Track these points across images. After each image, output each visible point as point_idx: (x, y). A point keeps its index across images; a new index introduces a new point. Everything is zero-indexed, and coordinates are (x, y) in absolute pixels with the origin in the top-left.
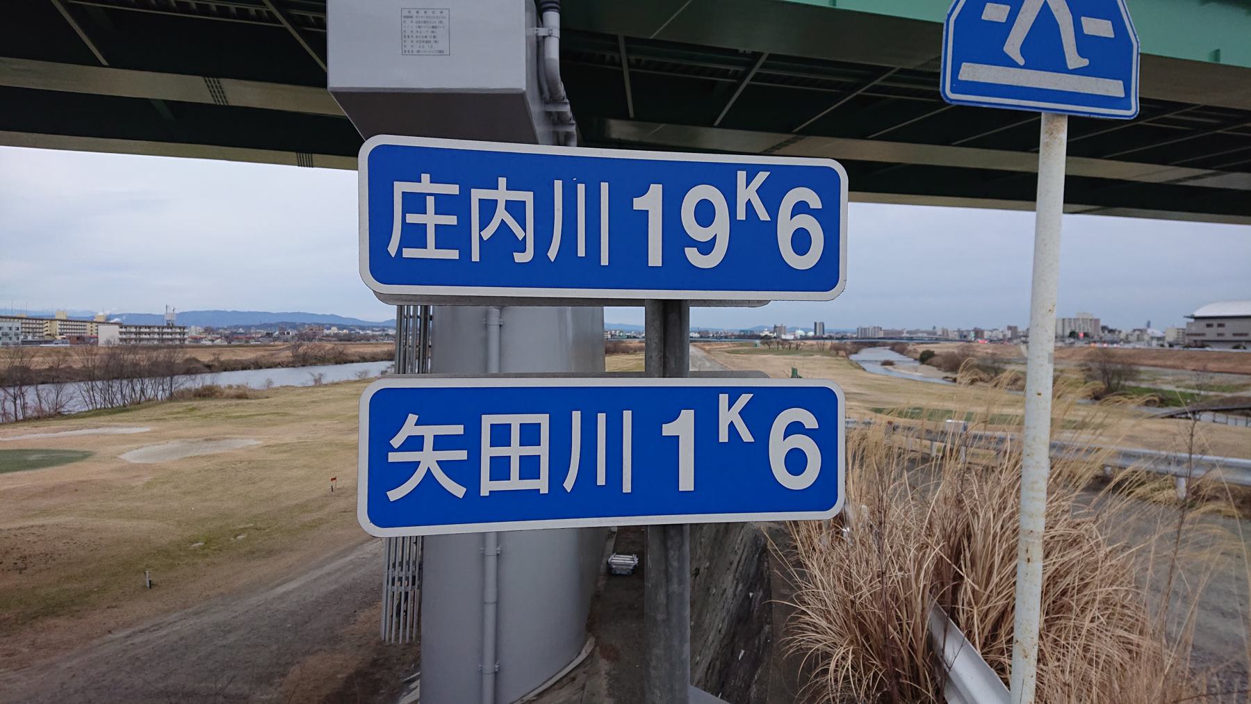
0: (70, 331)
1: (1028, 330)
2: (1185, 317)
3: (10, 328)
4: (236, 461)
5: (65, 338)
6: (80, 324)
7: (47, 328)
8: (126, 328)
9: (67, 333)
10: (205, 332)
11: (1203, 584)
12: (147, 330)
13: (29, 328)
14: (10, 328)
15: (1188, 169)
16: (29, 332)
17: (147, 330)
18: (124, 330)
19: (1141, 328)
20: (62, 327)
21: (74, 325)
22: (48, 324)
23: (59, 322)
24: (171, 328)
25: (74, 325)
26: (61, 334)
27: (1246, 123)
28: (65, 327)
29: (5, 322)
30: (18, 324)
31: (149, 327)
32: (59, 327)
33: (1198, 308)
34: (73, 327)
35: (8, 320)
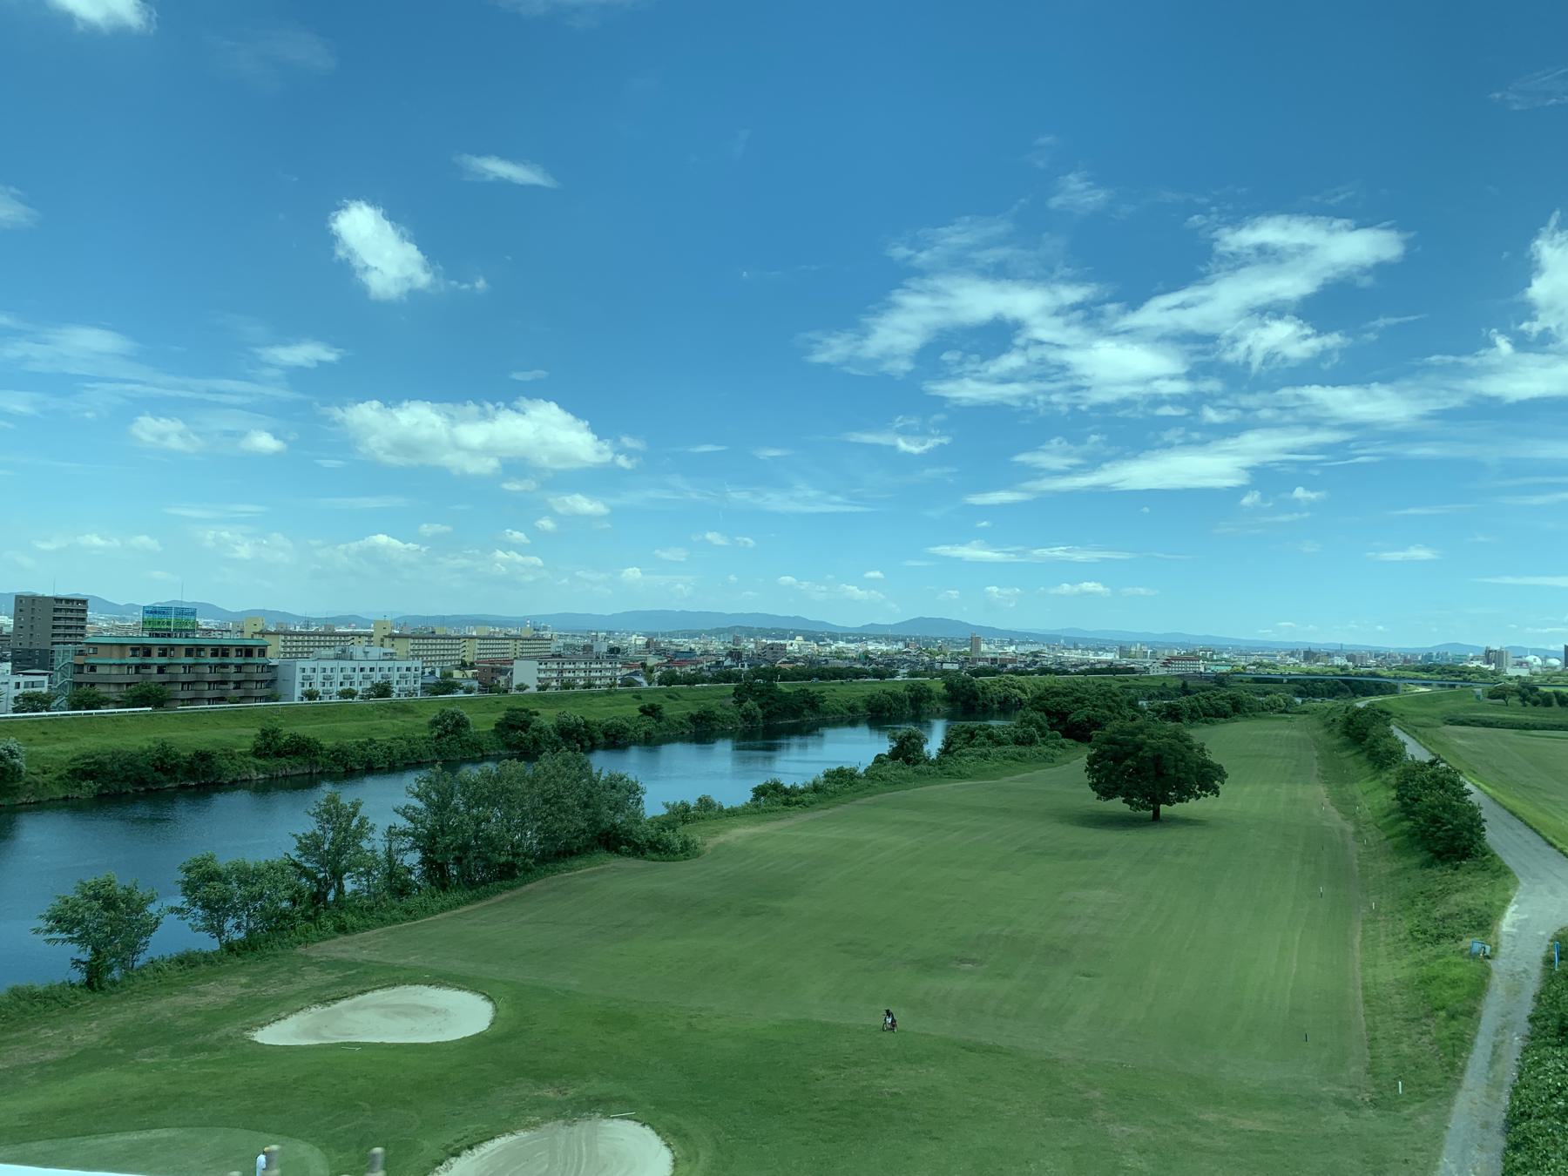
3: (408, 669)
14: (314, 670)
20: (482, 646)
22: (466, 644)
23: (478, 641)
32: (479, 646)
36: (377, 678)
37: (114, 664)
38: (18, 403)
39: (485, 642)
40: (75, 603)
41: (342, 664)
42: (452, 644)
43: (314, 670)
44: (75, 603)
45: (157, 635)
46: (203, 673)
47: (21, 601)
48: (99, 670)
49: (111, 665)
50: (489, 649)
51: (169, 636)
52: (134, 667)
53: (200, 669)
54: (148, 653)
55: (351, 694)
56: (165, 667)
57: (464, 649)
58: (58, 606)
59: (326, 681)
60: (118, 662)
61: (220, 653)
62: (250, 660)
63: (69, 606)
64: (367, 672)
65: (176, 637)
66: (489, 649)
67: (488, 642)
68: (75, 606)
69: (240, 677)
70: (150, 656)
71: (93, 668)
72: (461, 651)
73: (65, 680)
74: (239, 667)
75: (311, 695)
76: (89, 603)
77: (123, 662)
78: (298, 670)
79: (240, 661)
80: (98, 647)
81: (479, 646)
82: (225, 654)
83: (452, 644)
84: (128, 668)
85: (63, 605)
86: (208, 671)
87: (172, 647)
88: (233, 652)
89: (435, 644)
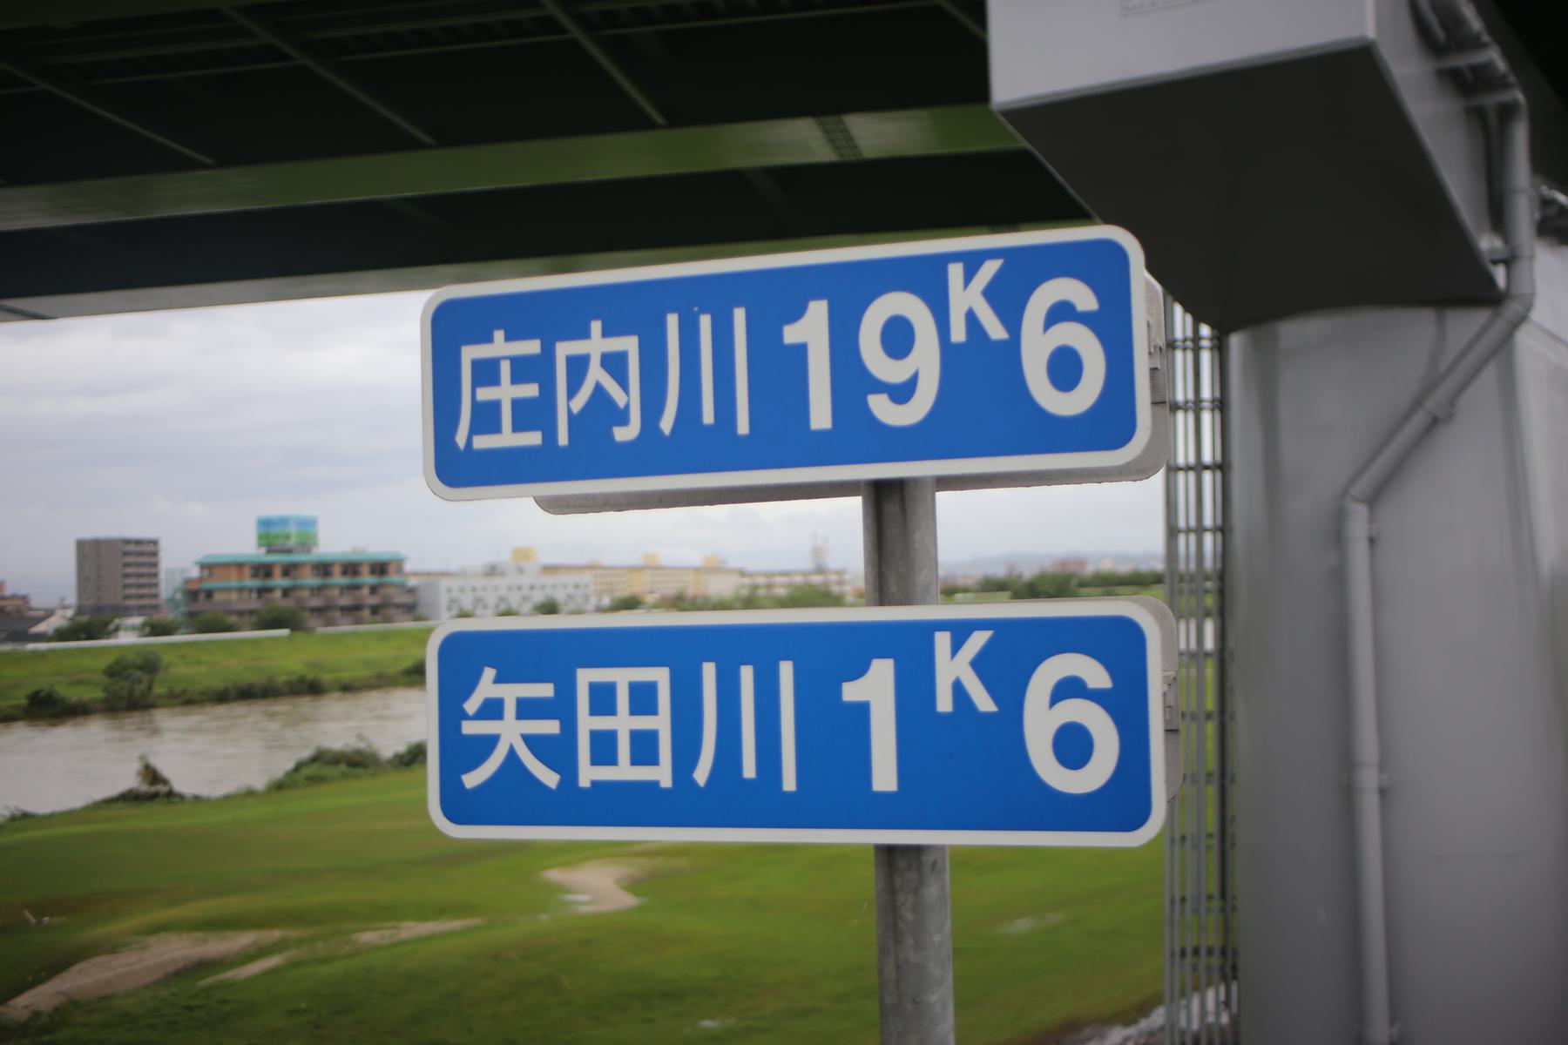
1: (142, 758)
3: (577, 586)
30: (587, 578)
41: (495, 581)
48: (218, 597)
69: (374, 600)
71: (209, 594)
85: (131, 548)
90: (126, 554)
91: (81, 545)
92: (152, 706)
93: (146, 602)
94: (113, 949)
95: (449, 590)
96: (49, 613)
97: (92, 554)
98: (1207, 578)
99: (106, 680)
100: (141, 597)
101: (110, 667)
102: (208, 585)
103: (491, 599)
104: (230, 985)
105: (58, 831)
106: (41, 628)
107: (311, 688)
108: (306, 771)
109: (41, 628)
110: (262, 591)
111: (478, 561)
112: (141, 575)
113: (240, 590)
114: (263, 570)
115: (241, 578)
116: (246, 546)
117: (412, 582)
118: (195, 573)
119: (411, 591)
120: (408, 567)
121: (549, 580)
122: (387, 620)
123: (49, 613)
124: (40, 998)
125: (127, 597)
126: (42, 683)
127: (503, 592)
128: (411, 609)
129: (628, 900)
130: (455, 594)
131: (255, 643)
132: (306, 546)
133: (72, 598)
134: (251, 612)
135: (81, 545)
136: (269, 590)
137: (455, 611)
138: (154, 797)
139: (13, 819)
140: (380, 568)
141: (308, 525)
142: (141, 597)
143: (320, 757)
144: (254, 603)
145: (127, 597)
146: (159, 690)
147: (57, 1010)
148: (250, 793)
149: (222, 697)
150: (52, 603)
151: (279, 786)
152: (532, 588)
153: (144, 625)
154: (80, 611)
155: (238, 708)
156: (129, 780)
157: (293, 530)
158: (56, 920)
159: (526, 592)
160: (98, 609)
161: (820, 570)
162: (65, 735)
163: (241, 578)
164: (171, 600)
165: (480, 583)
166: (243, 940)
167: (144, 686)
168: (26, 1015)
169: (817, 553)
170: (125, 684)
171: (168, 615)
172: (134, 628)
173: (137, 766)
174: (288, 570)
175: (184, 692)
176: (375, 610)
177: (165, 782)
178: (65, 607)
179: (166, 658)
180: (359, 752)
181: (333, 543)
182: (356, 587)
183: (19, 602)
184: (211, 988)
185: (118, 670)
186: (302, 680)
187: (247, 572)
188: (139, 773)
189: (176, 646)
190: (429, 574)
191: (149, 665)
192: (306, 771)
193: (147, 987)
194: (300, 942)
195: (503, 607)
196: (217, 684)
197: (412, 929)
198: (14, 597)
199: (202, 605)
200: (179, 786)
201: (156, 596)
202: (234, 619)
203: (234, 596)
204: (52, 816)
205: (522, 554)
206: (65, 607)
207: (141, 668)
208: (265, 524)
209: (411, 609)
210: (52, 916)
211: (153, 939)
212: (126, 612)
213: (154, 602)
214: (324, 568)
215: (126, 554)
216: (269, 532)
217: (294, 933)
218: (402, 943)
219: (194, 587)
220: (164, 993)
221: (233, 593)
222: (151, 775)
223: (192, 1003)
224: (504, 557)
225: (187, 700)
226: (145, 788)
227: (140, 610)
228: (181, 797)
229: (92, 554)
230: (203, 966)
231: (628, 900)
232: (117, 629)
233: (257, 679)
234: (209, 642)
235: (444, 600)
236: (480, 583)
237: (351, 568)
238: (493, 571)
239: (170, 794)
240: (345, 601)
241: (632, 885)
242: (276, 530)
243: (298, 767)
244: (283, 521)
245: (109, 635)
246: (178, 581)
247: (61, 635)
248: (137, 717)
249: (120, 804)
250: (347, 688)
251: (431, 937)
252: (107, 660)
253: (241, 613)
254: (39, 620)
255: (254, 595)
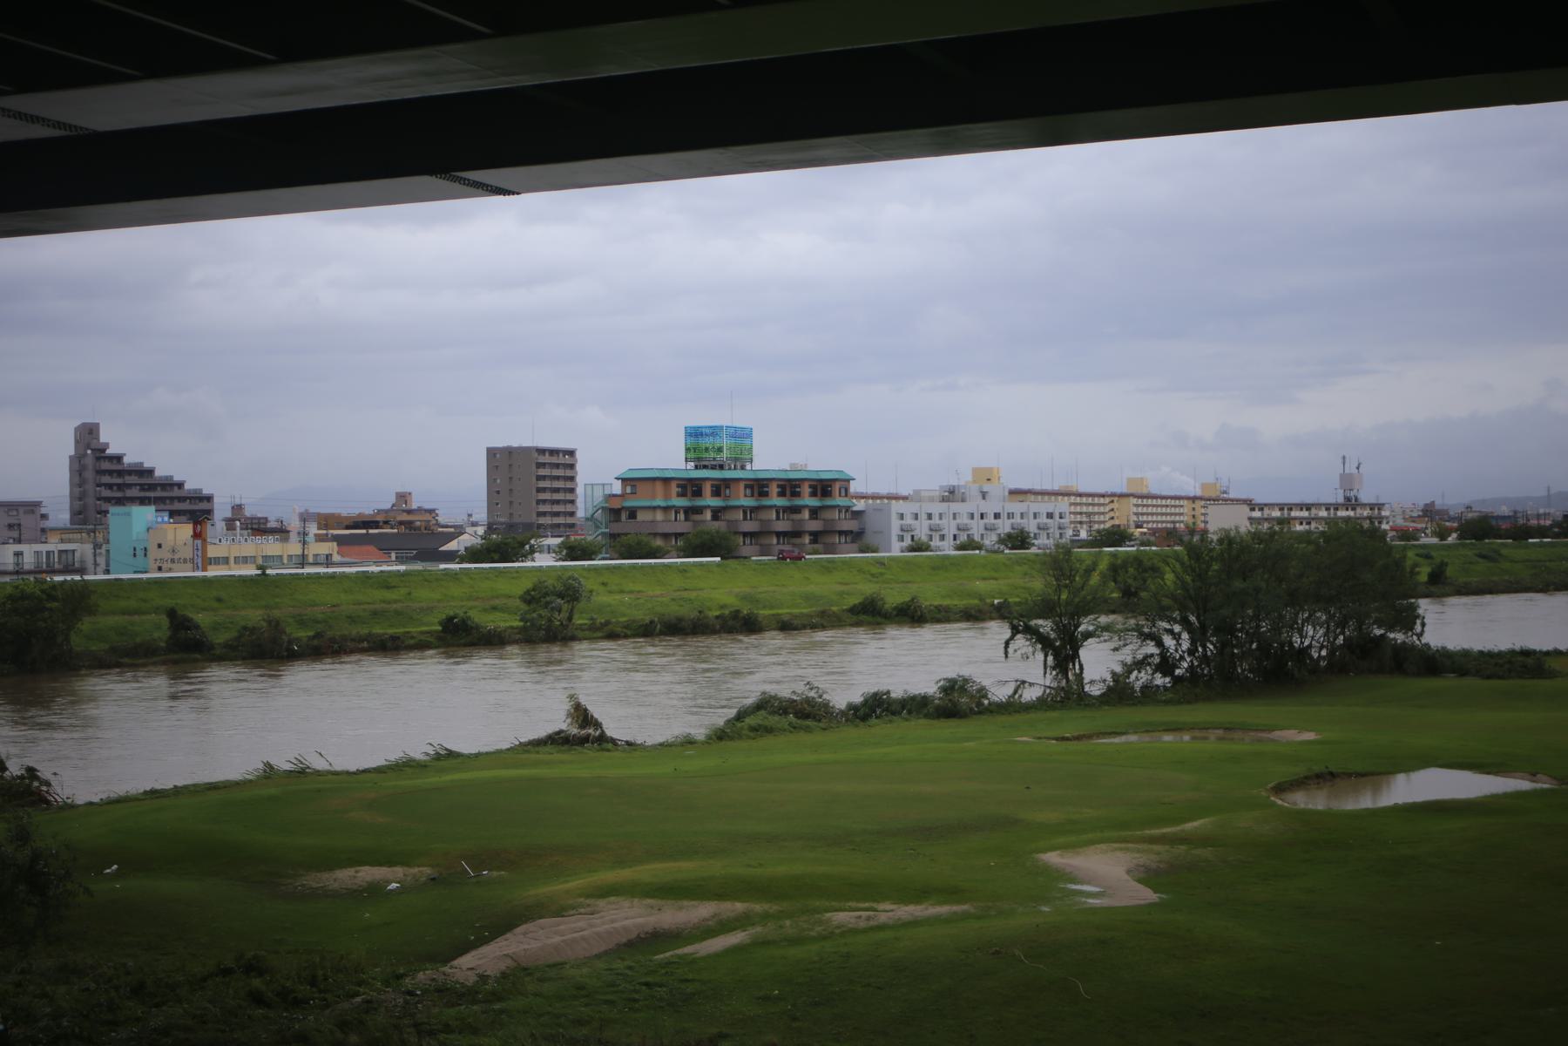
0: (1155, 518)
1: (571, 697)
2: (1006, 657)
3: (1050, 516)
4: (624, 751)
5: (1145, 533)
6: (1173, 502)
7: (1112, 514)
8: (1308, 509)
9: (1148, 522)
10: (1424, 516)
11: (557, 939)
12: (1305, 514)
13: (1081, 513)
14: (916, 517)
15: (1491, 778)
16: (1081, 523)
17: (1305, 514)
18: (1257, 514)
19: (1425, 635)
20: (1140, 510)
21: (1162, 506)
22: (1115, 506)
23: (1134, 501)
24: (1354, 509)
25: (1162, 506)
26: (1138, 526)
27: (679, 947)
28: (1145, 510)
29: (1050, 501)
30: (1063, 505)
31: (1308, 507)
32: (1135, 510)
33: (718, 565)
34: (1159, 510)
35: (1046, 498)
36: (1005, 527)
37: (659, 507)
38: (2, 722)
39: (1145, 501)
40: (561, 455)
41: (955, 507)
42: (1093, 505)
43: (916, 517)
44: (561, 455)
45: (705, 467)
46: (769, 520)
47: (495, 455)
48: (641, 516)
49: (654, 508)
50: (1152, 514)
51: (721, 467)
52: (682, 512)
53: (764, 515)
54: (698, 493)
55: (970, 545)
56: (719, 511)
57: (1112, 514)
58: (542, 459)
59: (905, 534)
60: (663, 504)
61: (788, 493)
62: (829, 502)
63: (554, 460)
64: (990, 520)
65: (730, 469)
66: (1152, 514)
67: (1150, 502)
68: (561, 460)
69: (815, 526)
70: (701, 495)
71: (632, 514)
72: (1108, 517)
73: (600, 531)
74: (815, 512)
75: (917, 547)
76: (578, 455)
77: (670, 503)
78: (894, 517)
79: (814, 502)
80: (638, 484)
81: (1135, 510)
82: (795, 494)
83: (1093, 505)
84: (676, 513)
85: (547, 459)
86: (774, 516)
87: (727, 482)
88: (806, 490)
89: (1080, 504)
90: (540, 465)
91: (492, 453)
92: (573, 638)
93: (560, 520)
94: (560, 912)
95: (902, 517)
96: (459, 531)
97: (503, 462)
98: (1276, 630)
99: (524, 607)
100: (557, 514)
101: (528, 592)
102: (629, 504)
103: (950, 528)
104: (691, 962)
105: (433, 780)
106: (452, 546)
107: (744, 624)
108: (750, 721)
109: (452, 546)
110: (690, 512)
111: (934, 483)
112: (557, 490)
113: (666, 509)
114: (691, 487)
115: (100, 554)
116: (672, 458)
117: (859, 505)
118: (617, 488)
119: (858, 515)
120: (854, 487)
121: (1016, 507)
122: (830, 549)
123: (459, 531)
124: (469, 965)
125: (540, 514)
126: (455, 608)
127: (965, 520)
128: (856, 537)
129: (1148, 896)
130: (909, 520)
131: (683, 570)
132: (740, 461)
133: (481, 515)
134: (677, 535)
135: (492, 453)
136: (699, 510)
137: (908, 542)
138: (583, 740)
139: (438, 757)
140: (823, 487)
141: (742, 435)
142: (557, 514)
143: (765, 704)
144: (682, 526)
145: (540, 514)
146: (579, 620)
147: (504, 975)
148: (689, 742)
149: (646, 631)
150: (460, 519)
151: (719, 735)
152: (997, 516)
153: (561, 546)
154: (490, 528)
155: (656, 652)
156: (557, 719)
157: (726, 442)
158: (495, 874)
159: (990, 520)
160: (511, 527)
161: (1351, 503)
162: (481, 664)
163: (667, 497)
164: (591, 519)
165: (937, 508)
166: (703, 911)
167: (564, 615)
168: (471, 979)
169: (1347, 480)
170: (544, 612)
171: (590, 537)
172: (549, 549)
173: (567, 706)
174: (720, 488)
175: (607, 623)
176: (816, 536)
177: (597, 725)
178: (474, 524)
179: (589, 584)
180: (809, 701)
181: (768, 459)
182: (796, 510)
183: (427, 517)
184: (669, 963)
185: (535, 597)
186: (736, 614)
187: (674, 489)
188: (569, 715)
189: (596, 569)
190: (874, 497)
191: (570, 593)
192: (750, 721)
193: (598, 956)
194: (765, 917)
195: (963, 538)
196: (642, 616)
197: (892, 912)
198: (420, 510)
199: (624, 525)
200: (609, 733)
201: (572, 514)
202: (659, 542)
203: (659, 516)
204: (478, 755)
205: (985, 476)
206: (474, 524)
207: (561, 596)
208: (694, 433)
209: (856, 537)
210: (489, 870)
211: (601, 903)
212: (539, 530)
213: (569, 520)
214: (759, 486)
215: (540, 465)
216: (698, 441)
217: (758, 907)
218: (881, 927)
219: (616, 505)
220: (619, 965)
221: (657, 512)
222: (582, 716)
223: (649, 979)
224: (962, 478)
225: (610, 632)
226: (575, 731)
227: (555, 529)
228: (613, 741)
229: (503, 462)
230: (657, 938)
231: (1148, 896)
232: (532, 551)
233: (687, 611)
234: (634, 567)
235: (895, 525)
236: (937, 508)
237: (790, 487)
238: (951, 494)
239: (602, 739)
240: (783, 526)
241: (1148, 877)
242: (707, 442)
243: (740, 717)
244: (715, 431)
245: (525, 557)
246: (599, 496)
247: (474, 555)
248: (556, 651)
249: (549, 748)
250: (786, 627)
251: (915, 923)
252: (526, 584)
253: (666, 536)
254: (452, 537)
255: (682, 516)
